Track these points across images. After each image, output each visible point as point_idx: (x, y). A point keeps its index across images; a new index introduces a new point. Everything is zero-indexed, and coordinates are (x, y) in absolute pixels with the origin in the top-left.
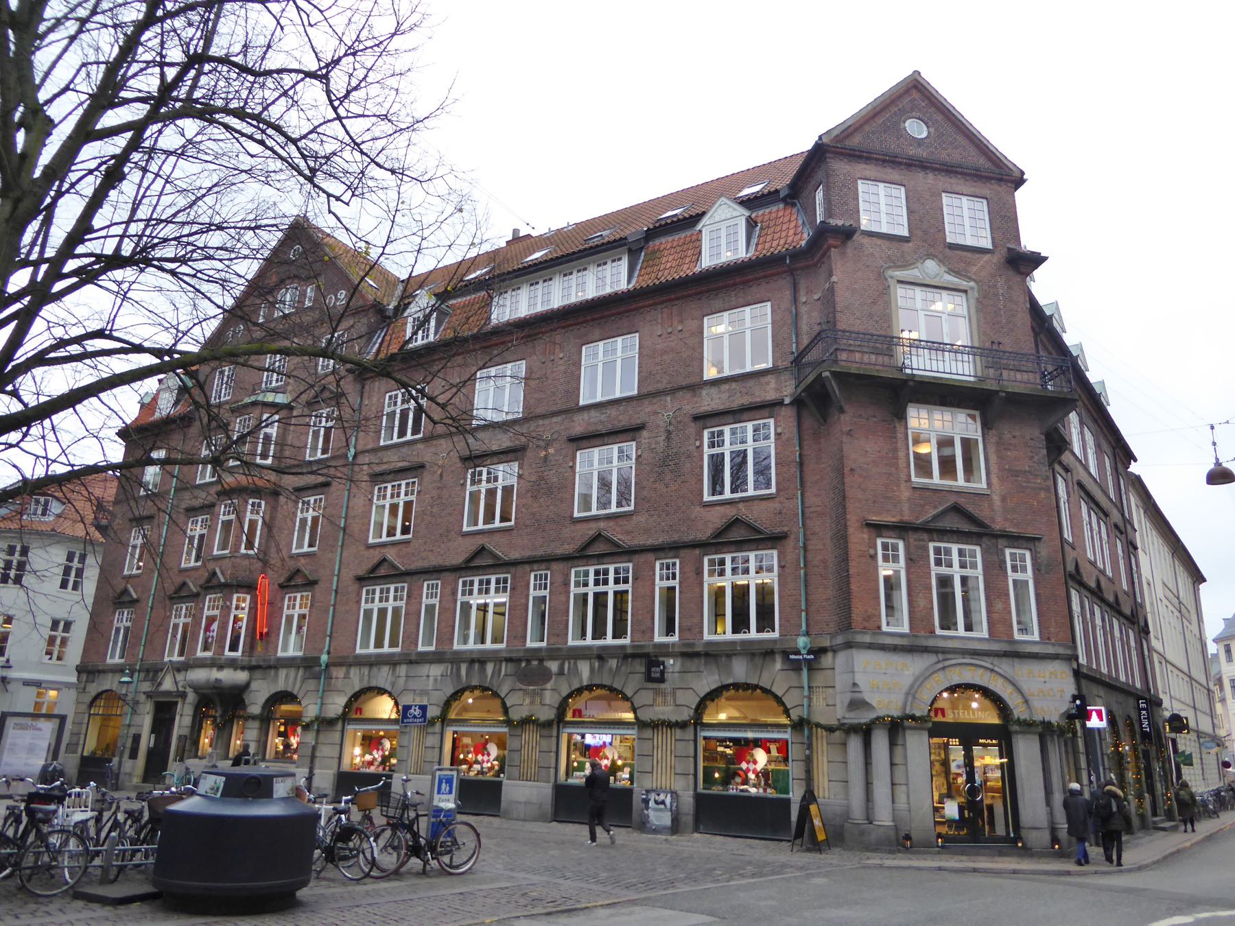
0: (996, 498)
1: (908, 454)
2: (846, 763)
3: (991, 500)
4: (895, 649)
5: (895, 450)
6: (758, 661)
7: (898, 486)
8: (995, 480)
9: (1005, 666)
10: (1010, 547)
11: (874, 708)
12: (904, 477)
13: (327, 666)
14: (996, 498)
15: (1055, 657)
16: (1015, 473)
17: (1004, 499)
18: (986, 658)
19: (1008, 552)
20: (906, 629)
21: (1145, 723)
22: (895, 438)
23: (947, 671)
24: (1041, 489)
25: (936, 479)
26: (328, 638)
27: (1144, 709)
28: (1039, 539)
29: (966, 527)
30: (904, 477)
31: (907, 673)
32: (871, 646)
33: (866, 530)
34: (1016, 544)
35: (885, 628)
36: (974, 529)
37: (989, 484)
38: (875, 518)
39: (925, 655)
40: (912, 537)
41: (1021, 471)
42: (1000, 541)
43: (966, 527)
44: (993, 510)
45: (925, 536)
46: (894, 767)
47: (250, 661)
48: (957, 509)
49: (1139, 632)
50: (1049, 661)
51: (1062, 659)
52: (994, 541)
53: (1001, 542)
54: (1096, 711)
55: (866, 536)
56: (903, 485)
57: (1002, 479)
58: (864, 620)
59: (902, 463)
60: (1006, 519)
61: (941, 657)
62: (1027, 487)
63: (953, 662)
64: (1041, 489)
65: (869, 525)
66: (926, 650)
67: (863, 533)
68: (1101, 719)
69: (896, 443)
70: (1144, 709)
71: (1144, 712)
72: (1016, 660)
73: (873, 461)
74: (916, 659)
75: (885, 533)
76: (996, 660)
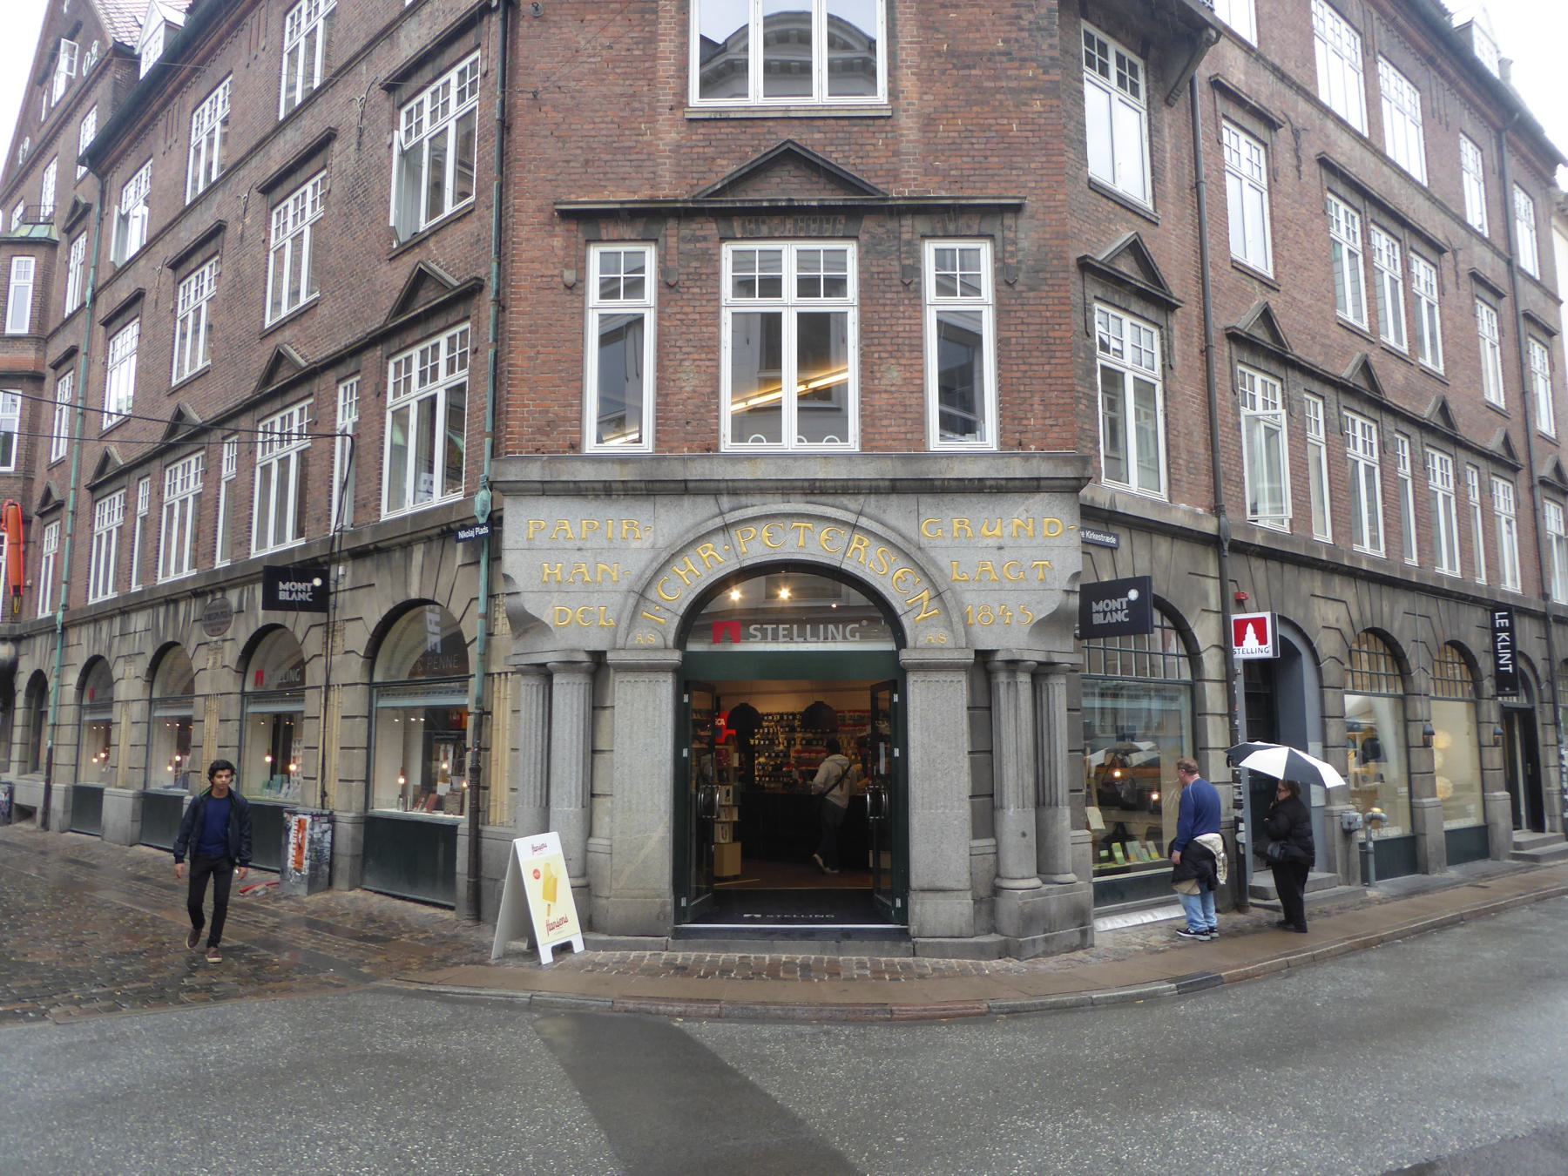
0: (909, 127)
1: (685, 46)
2: (991, 752)
3: (895, 128)
4: (606, 491)
5: (652, 39)
6: (436, 545)
7: (652, 121)
8: (908, 83)
9: (896, 513)
10: (934, 237)
11: (546, 626)
12: (666, 97)
13: (64, 628)
14: (909, 127)
15: (1032, 486)
16: (961, 59)
17: (928, 123)
18: (845, 500)
19: (929, 249)
20: (648, 446)
21: (1506, 656)
22: (655, 12)
23: (736, 534)
24: (1033, 90)
25: (756, 94)
26: (64, 586)
27: (1503, 630)
28: (1017, 209)
29: (812, 194)
30: (666, 97)
31: (635, 544)
32: (546, 489)
33: (559, 229)
34: (951, 228)
35: (590, 446)
36: (836, 198)
37: (893, 93)
38: (585, 199)
39: (687, 502)
40: (673, 232)
41: (980, 54)
42: (907, 222)
43: (812, 194)
44: (896, 153)
45: (711, 229)
46: (598, 757)
47: (11, 629)
48: (790, 157)
49: (1532, 489)
50: (1016, 497)
51: (1051, 490)
52: (892, 225)
53: (908, 227)
54: (1253, 621)
55: (557, 242)
56: (664, 118)
57: (926, 79)
58: (540, 431)
59: (665, 68)
60: (929, 171)
61: (726, 502)
62: (998, 90)
63: (749, 512)
64: (1033, 90)
65: (566, 215)
66: (684, 489)
67: (552, 236)
68: (1262, 639)
69: (655, 23)
70: (1503, 630)
71: (1504, 635)
72: (926, 500)
73: (595, 72)
74: (661, 511)
75: (607, 230)
76: (871, 504)
